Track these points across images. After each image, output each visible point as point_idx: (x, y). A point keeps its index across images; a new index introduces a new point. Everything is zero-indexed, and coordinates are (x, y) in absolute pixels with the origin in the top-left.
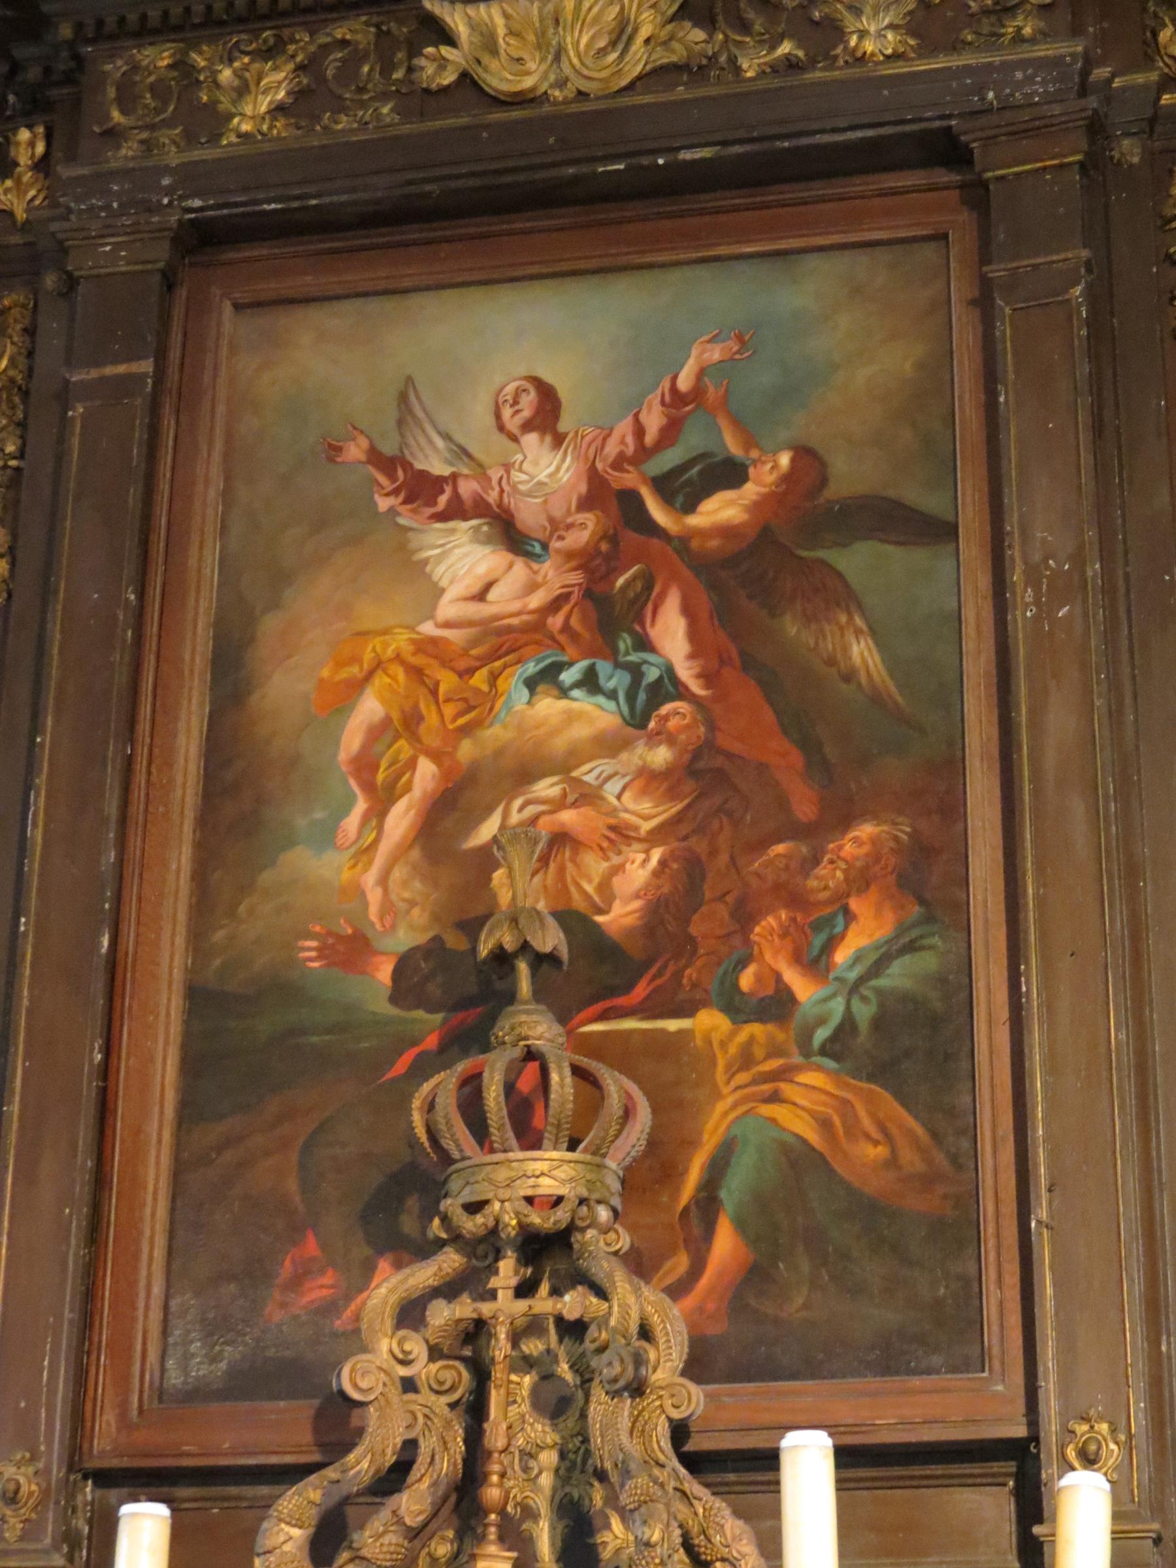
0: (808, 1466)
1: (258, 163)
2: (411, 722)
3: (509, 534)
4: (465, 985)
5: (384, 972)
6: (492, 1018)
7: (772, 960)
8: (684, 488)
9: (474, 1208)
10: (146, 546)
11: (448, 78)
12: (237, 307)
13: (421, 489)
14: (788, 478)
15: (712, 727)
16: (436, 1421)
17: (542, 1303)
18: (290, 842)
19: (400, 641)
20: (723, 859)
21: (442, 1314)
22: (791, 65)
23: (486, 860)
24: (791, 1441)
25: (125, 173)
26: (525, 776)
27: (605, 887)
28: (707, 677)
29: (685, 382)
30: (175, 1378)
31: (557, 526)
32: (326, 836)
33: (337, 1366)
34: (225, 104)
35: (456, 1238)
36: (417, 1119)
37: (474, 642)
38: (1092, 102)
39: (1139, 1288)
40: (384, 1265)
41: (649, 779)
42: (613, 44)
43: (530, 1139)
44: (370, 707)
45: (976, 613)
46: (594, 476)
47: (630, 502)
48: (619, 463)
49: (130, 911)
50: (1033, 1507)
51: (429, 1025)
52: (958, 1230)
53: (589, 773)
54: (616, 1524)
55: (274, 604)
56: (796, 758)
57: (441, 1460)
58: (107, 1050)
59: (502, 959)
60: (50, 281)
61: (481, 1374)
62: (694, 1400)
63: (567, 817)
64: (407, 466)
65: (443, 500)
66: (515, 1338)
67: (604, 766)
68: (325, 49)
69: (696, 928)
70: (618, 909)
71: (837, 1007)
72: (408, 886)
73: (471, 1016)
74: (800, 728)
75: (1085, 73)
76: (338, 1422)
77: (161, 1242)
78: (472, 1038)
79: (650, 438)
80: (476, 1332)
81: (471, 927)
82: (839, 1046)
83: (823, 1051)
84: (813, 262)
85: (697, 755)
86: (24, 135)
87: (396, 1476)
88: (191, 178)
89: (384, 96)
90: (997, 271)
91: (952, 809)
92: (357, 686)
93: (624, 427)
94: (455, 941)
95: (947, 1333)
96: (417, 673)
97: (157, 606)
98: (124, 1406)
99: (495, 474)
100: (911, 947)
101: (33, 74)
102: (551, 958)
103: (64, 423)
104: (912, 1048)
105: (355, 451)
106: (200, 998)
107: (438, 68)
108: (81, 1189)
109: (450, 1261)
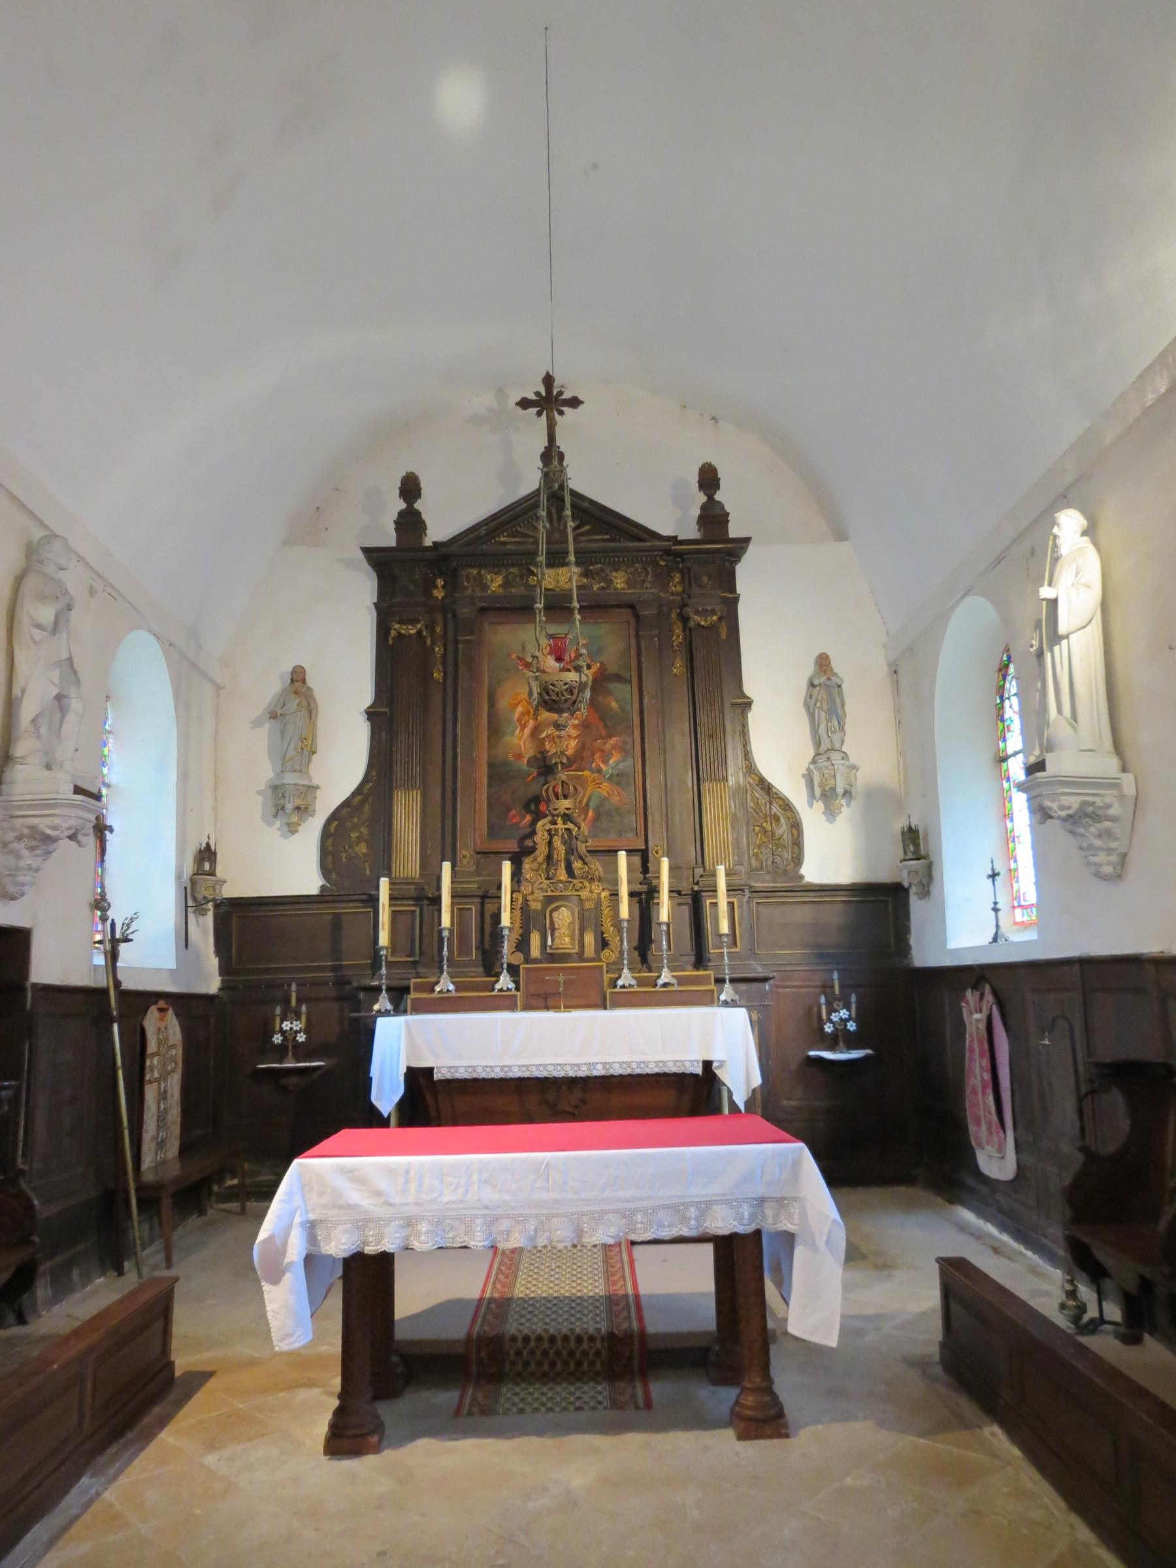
1: (495, 597)
7: (598, 762)
16: (588, 793)
22: (603, 588)
23: (543, 740)
43: (566, 797)
44: (520, 709)
72: (529, 744)
88: (482, 599)
92: (516, 706)
105: (514, 656)
106: (491, 765)
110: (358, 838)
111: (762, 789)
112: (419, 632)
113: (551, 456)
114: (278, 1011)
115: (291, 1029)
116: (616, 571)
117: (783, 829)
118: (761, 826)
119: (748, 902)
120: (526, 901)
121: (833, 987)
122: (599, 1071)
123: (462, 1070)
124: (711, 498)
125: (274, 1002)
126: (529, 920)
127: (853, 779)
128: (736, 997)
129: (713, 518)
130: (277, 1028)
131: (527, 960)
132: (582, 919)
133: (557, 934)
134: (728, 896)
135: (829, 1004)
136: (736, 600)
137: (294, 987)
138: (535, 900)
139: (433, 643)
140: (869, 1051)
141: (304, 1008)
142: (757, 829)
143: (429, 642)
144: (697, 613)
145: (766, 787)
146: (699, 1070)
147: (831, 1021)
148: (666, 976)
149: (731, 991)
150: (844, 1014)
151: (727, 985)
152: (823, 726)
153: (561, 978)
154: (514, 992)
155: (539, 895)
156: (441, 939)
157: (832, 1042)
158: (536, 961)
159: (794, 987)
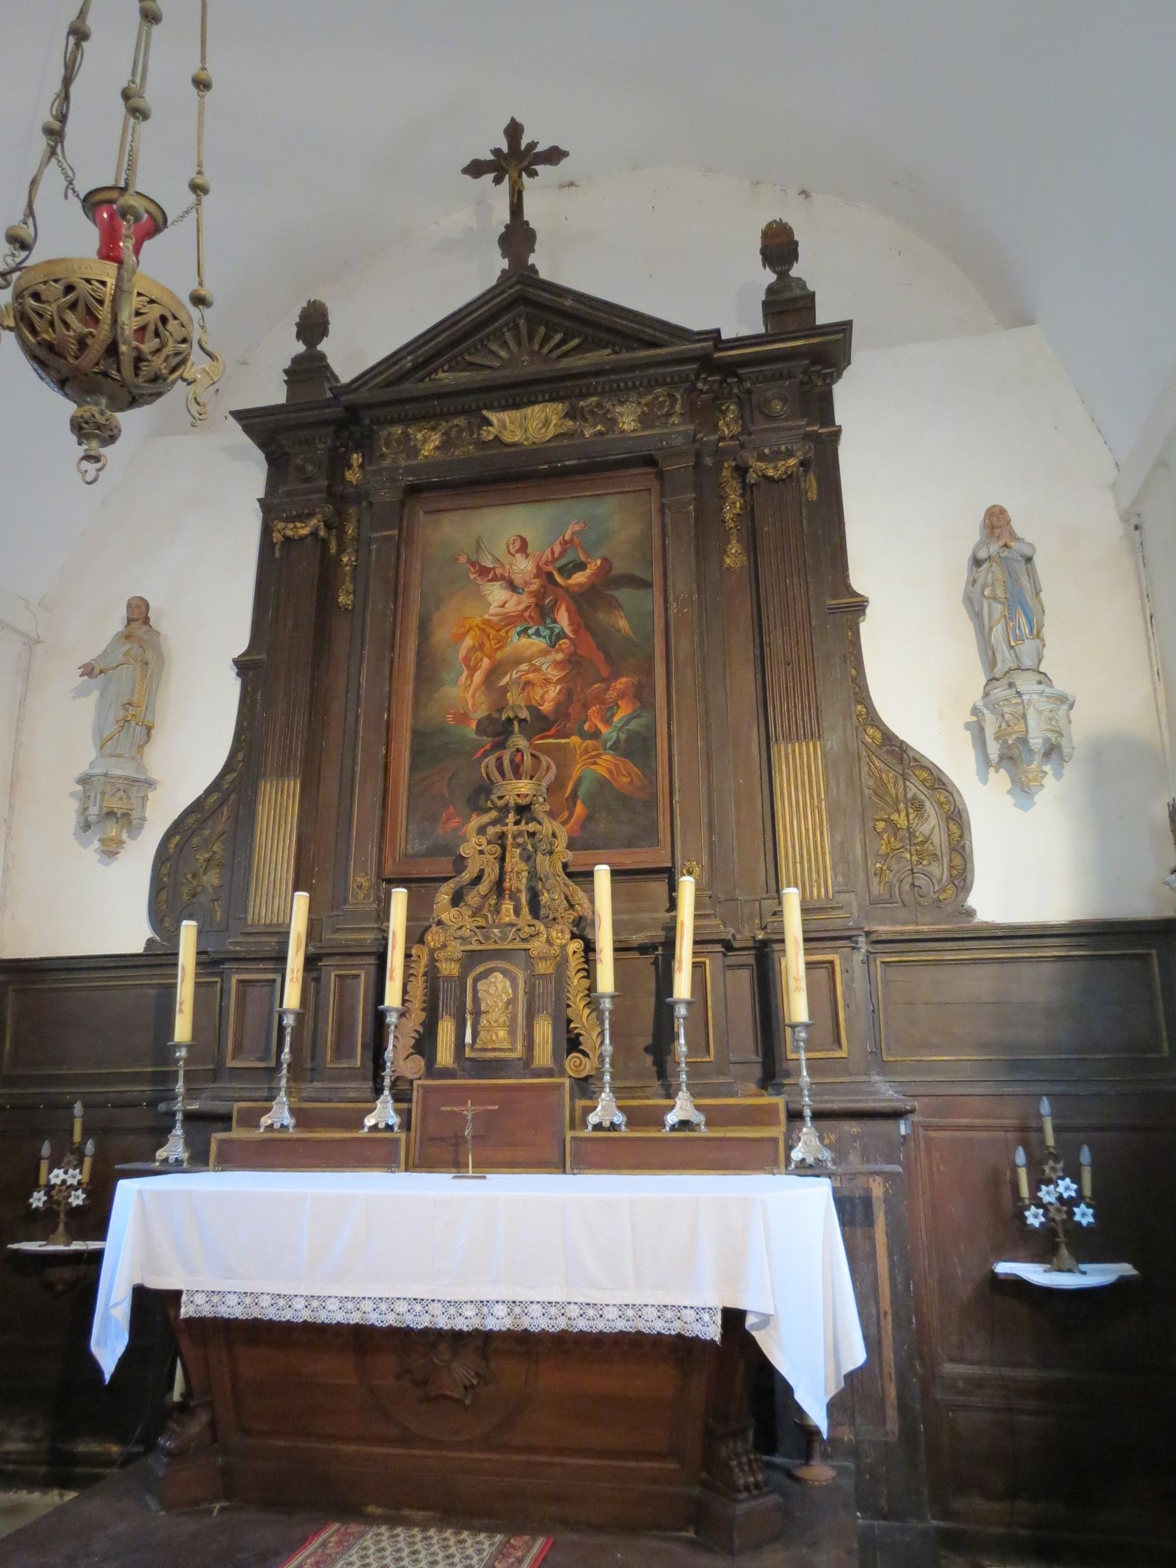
0: (603, 875)
1: (431, 466)
2: (481, 646)
3: (512, 586)
4: (499, 729)
5: (474, 725)
6: (506, 740)
7: (594, 719)
8: (568, 570)
9: (501, 798)
10: (396, 590)
11: (491, 437)
12: (425, 513)
13: (484, 572)
14: (601, 568)
15: (575, 646)
16: (575, 774)
17: (522, 827)
18: (443, 685)
19: (478, 620)
20: (579, 688)
21: (491, 831)
22: (601, 433)
23: (505, 689)
24: (597, 867)
25: (387, 469)
26: (518, 663)
27: (542, 697)
28: (575, 632)
29: (567, 538)
30: (410, 851)
31: (527, 583)
32: (455, 682)
33: (459, 846)
34: (419, 446)
35: (495, 807)
36: (483, 770)
37: (501, 621)
38: (697, 445)
39: (706, 820)
40: (474, 815)
41: (557, 664)
42: (543, 426)
43: (518, 775)
44: (468, 642)
45: (659, 611)
46: (538, 567)
47: (550, 576)
48: (546, 563)
49: (393, 707)
50: (673, 887)
51: (488, 742)
52: (651, 804)
53: (537, 662)
54: (546, 894)
55: (437, 609)
56: (602, 656)
57: (491, 875)
58: (387, 749)
59: (509, 721)
60: (364, 504)
61: (504, 848)
62: (569, 856)
63: (531, 676)
64: (479, 564)
65: (491, 575)
66: (514, 838)
67: (542, 660)
68: (451, 428)
69: (570, 711)
70: (546, 705)
71: (614, 735)
72: (481, 698)
73: (501, 738)
74: (603, 647)
75: (695, 435)
76: (460, 863)
77: (405, 810)
78: (501, 746)
79: (556, 555)
80: (502, 836)
81: (500, 710)
82: (615, 747)
83: (610, 748)
84: (607, 498)
85: (571, 656)
86: (355, 456)
87: (477, 880)
88: (409, 470)
89: (470, 444)
90: (666, 501)
91: (650, 673)
92: (465, 635)
93: (548, 552)
94: (495, 715)
95: (647, 835)
96: (483, 630)
97: (470, 318)
98: (394, 858)
99: (507, 567)
100: (638, 716)
101: (357, 436)
102: (525, 720)
103: (370, 552)
104: (637, 747)
105: (463, 560)
106: (416, 733)
107: (488, 434)
108: (380, 793)
109: (494, 814)
110: (208, 860)
111: (891, 752)
112: (314, 534)
113: (518, 237)
114: (46, 1150)
115: (64, 1182)
116: (622, 403)
117: (931, 825)
118: (888, 821)
119: (867, 961)
120: (433, 961)
121: (1041, 1130)
122: (499, 1321)
123: (232, 1300)
124: (783, 275)
125: (40, 1135)
126: (438, 996)
127: (1062, 723)
128: (826, 1155)
129: (788, 304)
130: (42, 1181)
131: (432, 1071)
132: (531, 995)
133: (483, 1022)
134: (807, 951)
135: (1034, 1165)
136: (836, 434)
137: (78, 1109)
138: (450, 960)
139: (341, 550)
140: (1125, 1269)
141: (90, 1147)
142: (881, 825)
143: (333, 548)
144: (761, 457)
145: (895, 749)
146: (713, 1331)
147: (1039, 1204)
148: (682, 1108)
149: (815, 1141)
150: (1066, 1188)
151: (808, 1131)
152: (998, 631)
153: (469, 1110)
154: (399, 1134)
155: (456, 949)
156: (281, 1029)
157: (1043, 1246)
158: (447, 1073)
159: (959, 1128)
